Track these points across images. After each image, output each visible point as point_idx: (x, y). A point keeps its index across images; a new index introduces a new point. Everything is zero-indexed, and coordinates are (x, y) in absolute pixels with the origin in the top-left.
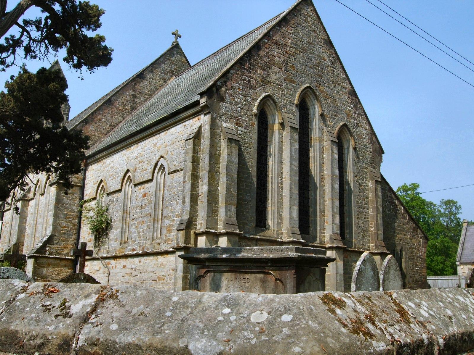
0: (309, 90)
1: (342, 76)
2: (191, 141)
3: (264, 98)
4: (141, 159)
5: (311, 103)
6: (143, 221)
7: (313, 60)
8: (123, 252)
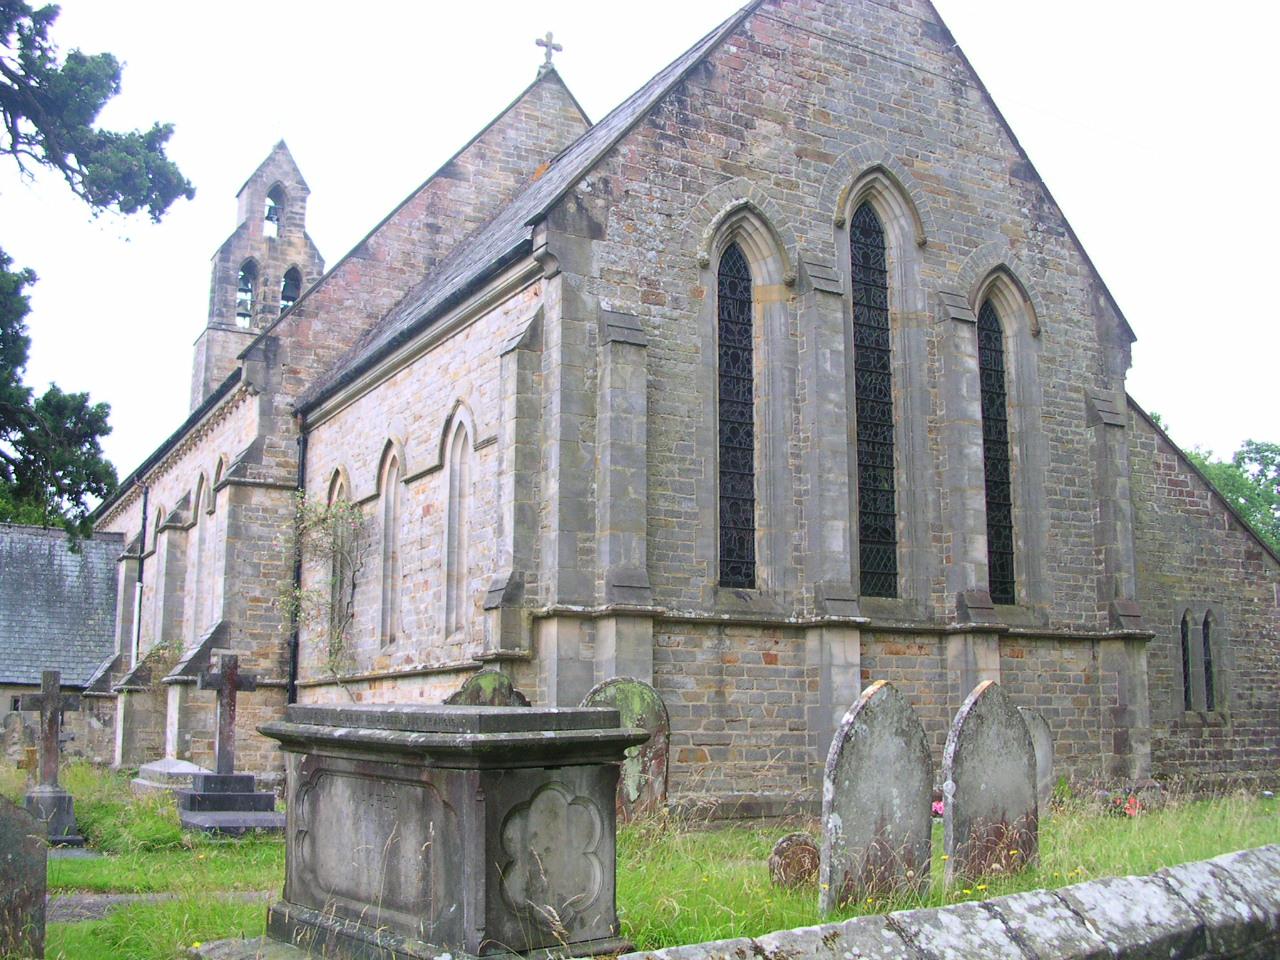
0: (880, 176)
1: (988, 126)
2: (513, 357)
3: (730, 215)
4: (417, 408)
5: (890, 213)
6: (426, 582)
7: (889, 85)
8: (387, 667)
